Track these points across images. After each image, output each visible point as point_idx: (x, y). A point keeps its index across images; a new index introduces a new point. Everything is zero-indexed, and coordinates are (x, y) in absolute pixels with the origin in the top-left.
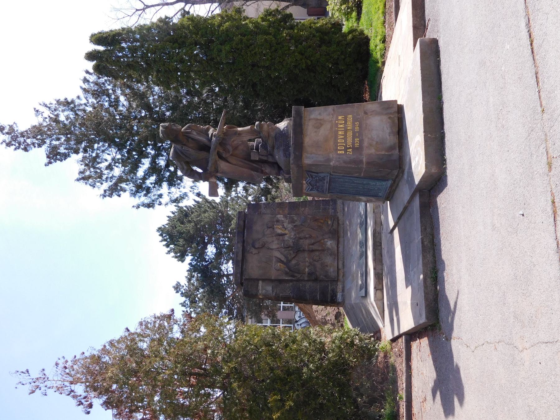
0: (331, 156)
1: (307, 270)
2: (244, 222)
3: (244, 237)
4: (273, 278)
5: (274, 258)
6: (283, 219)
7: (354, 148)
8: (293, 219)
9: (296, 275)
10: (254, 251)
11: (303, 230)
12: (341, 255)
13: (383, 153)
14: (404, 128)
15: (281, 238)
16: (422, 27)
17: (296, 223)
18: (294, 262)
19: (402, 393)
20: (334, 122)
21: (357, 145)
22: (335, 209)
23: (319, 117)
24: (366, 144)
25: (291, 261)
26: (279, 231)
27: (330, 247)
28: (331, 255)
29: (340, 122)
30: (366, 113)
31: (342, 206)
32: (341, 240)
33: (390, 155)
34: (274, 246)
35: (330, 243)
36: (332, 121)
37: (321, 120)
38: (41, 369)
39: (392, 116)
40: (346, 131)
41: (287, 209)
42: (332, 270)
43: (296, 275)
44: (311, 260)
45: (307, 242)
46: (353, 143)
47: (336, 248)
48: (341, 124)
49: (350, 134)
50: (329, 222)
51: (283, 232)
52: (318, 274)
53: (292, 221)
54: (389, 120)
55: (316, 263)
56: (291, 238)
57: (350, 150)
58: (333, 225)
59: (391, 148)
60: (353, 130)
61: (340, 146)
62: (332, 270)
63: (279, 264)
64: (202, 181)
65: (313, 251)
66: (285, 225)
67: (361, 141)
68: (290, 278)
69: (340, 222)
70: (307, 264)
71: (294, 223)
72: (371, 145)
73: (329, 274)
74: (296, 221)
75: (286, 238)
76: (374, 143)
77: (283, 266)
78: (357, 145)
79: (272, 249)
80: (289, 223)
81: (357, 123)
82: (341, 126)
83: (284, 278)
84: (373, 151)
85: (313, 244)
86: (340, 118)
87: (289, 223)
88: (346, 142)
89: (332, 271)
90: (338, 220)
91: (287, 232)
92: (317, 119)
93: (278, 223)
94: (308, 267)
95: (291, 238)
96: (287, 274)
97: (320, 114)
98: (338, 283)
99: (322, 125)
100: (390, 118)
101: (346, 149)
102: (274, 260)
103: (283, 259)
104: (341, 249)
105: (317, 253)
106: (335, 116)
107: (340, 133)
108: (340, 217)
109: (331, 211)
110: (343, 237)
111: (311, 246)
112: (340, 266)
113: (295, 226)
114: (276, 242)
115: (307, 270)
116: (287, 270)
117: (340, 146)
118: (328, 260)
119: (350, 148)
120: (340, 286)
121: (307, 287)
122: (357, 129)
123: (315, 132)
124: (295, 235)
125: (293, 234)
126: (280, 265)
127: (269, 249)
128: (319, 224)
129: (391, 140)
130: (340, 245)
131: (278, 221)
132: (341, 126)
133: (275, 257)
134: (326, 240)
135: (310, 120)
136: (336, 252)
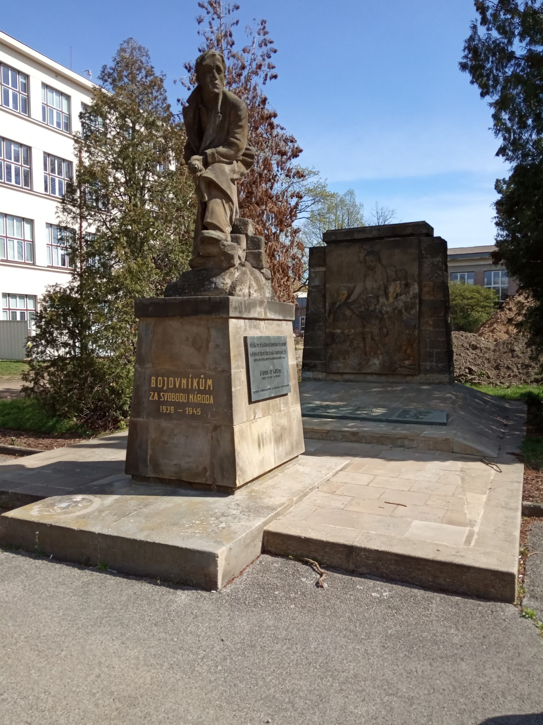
0: (149, 365)
1: (338, 331)
2: (412, 235)
3: (389, 237)
4: (327, 285)
5: (353, 285)
6: (411, 293)
7: (159, 403)
8: (412, 308)
9: (332, 317)
10: (362, 255)
11: (394, 323)
12: (360, 377)
13: (150, 452)
14: (183, 491)
15: (382, 292)
16: (352, 567)
17: (405, 313)
18: (348, 313)
19: (84, 442)
20: (203, 371)
21: (163, 409)
22: (431, 371)
23: (212, 345)
24: (165, 424)
25: (350, 308)
26: (391, 289)
27: (371, 363)
28: (360, 364)
29: (202, 382)
30: (216, 428)
31: (437, 381)
32: (383, 379)
33: (146, 461)
34: (370, 284)
35: (376, 363)
36: (205, 367)
37: (208, 348)
38: (238, 4)
39: (208, 474)
40: (187, 391)
41: (432, 298)
42: (340, 365)
43: (332, 317)
44: (352, 337)
45: (376, 331)
46: (166, 403)
47: (369, 371)
48: (198, 383)
49: (181, 398)
50: (407, 362)
51: (390, 295)
52: (334, 346)
53: (408, 307)
54: (201, 468)
55: (348, 343)
56: (382, 306)
57: (156, 398)
58: (401, 367)
59: (156, 466)
60: (188, 404)
61: (164, 380)
62: (340, 365)
63: (346, 292)
64: (436, 234)
65: (364, 339)
66: (403, 297)
67: (168, 416)
68: (327, 308)
69: (409, 378)
70: (346, 331)
71: (406, 310)
72: (162, 432)
73: (334, 362)
74: (409, 313)
75: (382, 300)
76: (165, 438)
77: (343, 298)
78: (163, 409)
79: (364, 282)
80: (405, 303)
81: (198, 412)
82: (195, 384)
83: (328, 301)
84: (153, 435)
85: (373, 339)
86: (210, 382)
87: (405, 303)
88: (169, 390)
89: (338, 365)
90: (412, 375)
91: (391, 300)
92: (208, 342)
93: (403, 286)
94: (343, 333)
95: (382, 306)
96: (334, 304)
97: (217, 346)
98: (324, 374)
99: (199, 349)
100: (205, 469)
101: (158, 390)
102: (351, 285)
103: (353, 297)
104: (369, 378)
105: (361, 345)
106: (213, 373)
107: (184, 381)
108: (417, 378)
109: (428, 365)
110: (387, 382)
111: (369, 336)
112: (346, 377)
113: (400, 312)
114: (375, 286)
115: (338, 331)
116: (338, 303)
117: (164, 380)
118: (353, 361)
119: (159, 397)
120: (321, 376)
121: (319, 333)
122: (189, 411)
123: (187, 339)
124: (387, 312)
125: (389, 309)
126: (344, 294)
127: (366, 276)
128: (404, 348)
129: (169, 467)
130: (375, 376)
131: (407, 285)
132: (195, 384)
133: (355, 287)
134: (381, 357)
135: (208, 328)
136: (364, 371)
